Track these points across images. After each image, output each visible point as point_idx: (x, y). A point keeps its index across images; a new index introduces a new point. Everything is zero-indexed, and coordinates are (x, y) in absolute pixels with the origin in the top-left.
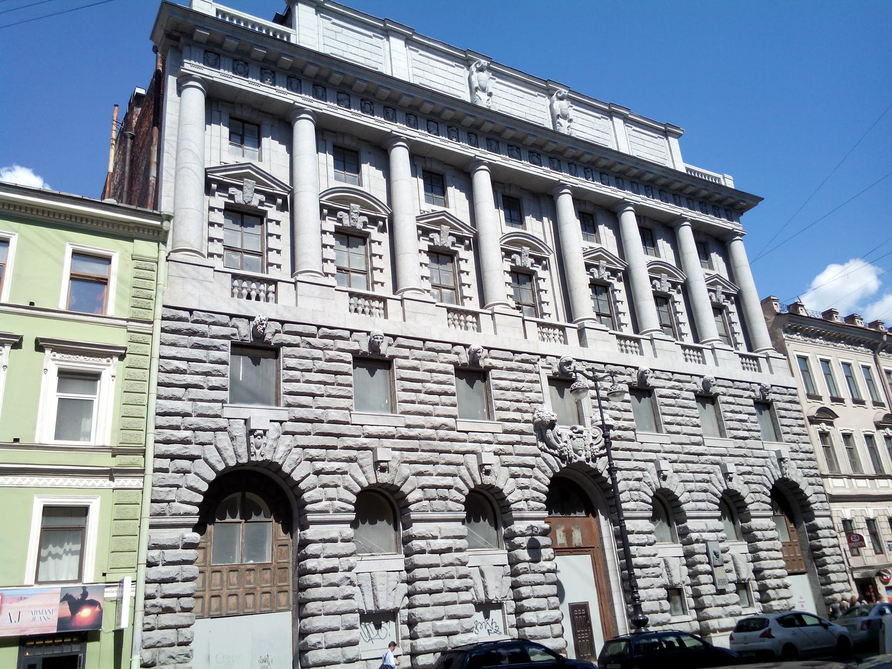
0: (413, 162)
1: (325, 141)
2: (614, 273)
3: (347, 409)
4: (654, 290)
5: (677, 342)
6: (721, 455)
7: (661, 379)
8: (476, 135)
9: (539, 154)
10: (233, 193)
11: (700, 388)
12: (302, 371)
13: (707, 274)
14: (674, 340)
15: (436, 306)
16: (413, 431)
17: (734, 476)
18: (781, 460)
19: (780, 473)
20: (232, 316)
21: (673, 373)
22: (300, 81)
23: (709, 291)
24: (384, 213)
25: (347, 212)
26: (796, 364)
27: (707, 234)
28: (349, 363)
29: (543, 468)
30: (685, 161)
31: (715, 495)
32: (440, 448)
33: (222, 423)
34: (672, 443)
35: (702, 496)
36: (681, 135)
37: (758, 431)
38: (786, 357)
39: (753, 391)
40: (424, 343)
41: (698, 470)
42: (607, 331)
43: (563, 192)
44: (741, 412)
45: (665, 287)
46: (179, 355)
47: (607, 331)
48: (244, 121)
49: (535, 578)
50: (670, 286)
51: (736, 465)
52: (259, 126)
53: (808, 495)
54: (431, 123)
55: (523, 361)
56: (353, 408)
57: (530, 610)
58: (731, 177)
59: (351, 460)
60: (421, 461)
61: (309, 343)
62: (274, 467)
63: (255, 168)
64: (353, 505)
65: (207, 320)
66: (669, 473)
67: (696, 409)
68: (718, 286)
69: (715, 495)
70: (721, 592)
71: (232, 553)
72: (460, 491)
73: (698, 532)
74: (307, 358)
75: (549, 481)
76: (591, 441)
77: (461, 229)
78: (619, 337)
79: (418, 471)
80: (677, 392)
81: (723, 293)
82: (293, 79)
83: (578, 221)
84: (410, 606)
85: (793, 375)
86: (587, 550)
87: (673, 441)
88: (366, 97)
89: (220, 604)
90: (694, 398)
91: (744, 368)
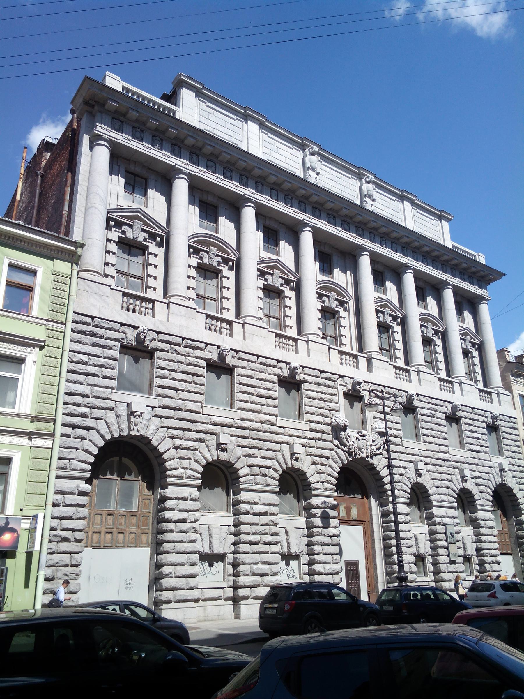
3: (200, 402)
6: (461, 462)
7: (423, 401)
9: (349, 223)
10: (125, 230)
17: (469, 478)
18: (502, 470)
19: (500, 480)
20: (122, 324)
21: (431, 398)
25: (207, 252)
28: (203, 368)
29: (335, 460)
30: (452, 239)
31: (454, 491)
32: (264, 438)
33: (111, 404)
34: (427, 450)
35: (445, 491)
36: (451, 220)
37: (487, 447)
38: (511, 395)
40: (258, 358)
46: (83, 351)
48: (135, 175)
50: (433, 332)
51: (470, 470)
52: (146, 180)
54: (273, 191)
55: (327, 379)
56: (204, 402)
58: (483, 256)
59: (200, 441)
61: (176, 350)
63: (143, 212)
64: (200, 474)
65: (104, 325)
66: (423, 472)
67: (445, 426)
68: (468, 337)
69: (454, 491)
72: (276, 470)
74: (174, 361)
77: (154, 226)
80: (433, 412)
85: (515, 408)
89: (100, 538)
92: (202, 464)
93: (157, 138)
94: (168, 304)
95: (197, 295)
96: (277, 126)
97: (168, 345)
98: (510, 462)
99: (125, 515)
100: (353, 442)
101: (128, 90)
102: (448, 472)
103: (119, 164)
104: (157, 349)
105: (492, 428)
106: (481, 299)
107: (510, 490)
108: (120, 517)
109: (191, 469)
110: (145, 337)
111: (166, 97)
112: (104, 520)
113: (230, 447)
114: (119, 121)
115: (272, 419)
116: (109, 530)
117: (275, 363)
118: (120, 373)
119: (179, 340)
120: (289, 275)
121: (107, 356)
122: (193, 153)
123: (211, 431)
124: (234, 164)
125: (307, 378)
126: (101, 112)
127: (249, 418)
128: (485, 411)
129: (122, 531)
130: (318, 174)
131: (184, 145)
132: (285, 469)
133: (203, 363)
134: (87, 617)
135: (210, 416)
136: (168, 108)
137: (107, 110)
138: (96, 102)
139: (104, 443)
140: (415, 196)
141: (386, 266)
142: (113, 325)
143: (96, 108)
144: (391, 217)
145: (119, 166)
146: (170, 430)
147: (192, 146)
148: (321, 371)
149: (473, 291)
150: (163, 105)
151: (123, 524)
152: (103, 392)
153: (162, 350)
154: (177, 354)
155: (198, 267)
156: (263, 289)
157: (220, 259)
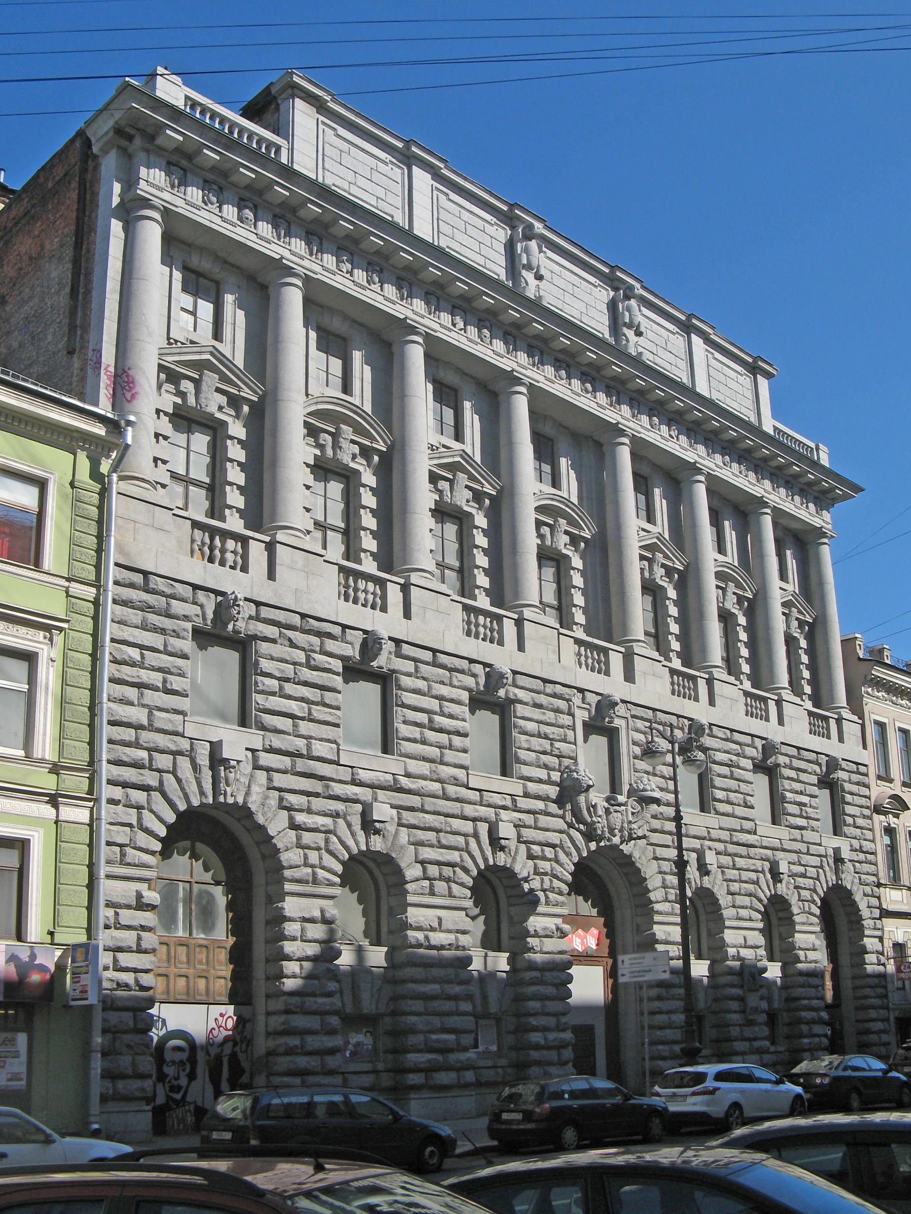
0: (169, 249)
1: (172, 257)
2: (234, 402)
3: (335, 742)
4: (179, 401)
5: (740, 687)
6: (773, 849)
7: (717, 737)
8: (514, 337)
9: (594, 379)
10: (185, 390)
11: (352, 651)
12: (279, 679)
13: (643, 530)
14: (737, 683)
15: (174, 515)
16: (414, 783)
17: (785, 878)
18: (838, 860)
19: (834, 878)
20: (196, 587)
21: (732, 730)
22: (289, 223)
23: (642, 558)
24: (587, 532)
26: (871, 731)
27: (725, 500)
28: (338, 674)
29: (567, 850)
30: (775, 416)
31: (760, 901)
32: (445, 811)
33: (185, 745)
34: (720, 828)
35: (746, 901)
36: (773, 375)
37: (818, 820)
38: (860, 722)
39: (475, 676)
41: (745, 867)
42: (660, 662)
43: (139, 213)
44: (801, 793)
45: (462, 498)
46: (131, 639)
47: (660, 662)
48: (199, 274)
49: (547, 991)
50: (735, 601)
51: (789, 863)
52: (217, 283)
53: (650, 887)
55: (555, 696)
56: (340, 741)
57: (536, 1029)
58: (825, 449)
59: (336, 815)
60: (422, 825)
61: (290, 640)
62: (244, 812)
63: (218, 355)
64: (339, 876)
65: (165, 590)
66: (713, 868)
68: (793, 609)
69: (760, 901)
70: (751, 1023)
71: (176, 928)
72: (466, 870)
73: (735, 947)
74: (287, 662)
75: (573, 868)
76: (630, 818)
77: (239, 383)
78: (466, 608)
79: (418, 838)
80: (734, 758)
81: (663, 566)
82: (281, 220)
83: (532, 446)
84: (394, 1013)
85: (865, 747)
86: (600, 959)
87: (722, 825)
88: (375, 259)
90: (341, 670)
91: (673, 693)
92: (341, 858)
93: (248, 203)
94: (307, 573)
95: (315, 524)
96: (465, 179)
97: (275, 630)
98: (851, 846)
99: (207, 947)
100: (600, 816)
101: (194, 104)
102: (753, 868)
103: (171, 254)
104: (255, 637)
105: (827, 782)
106: (819, 533)
107: (849, 893)
108: (198, 949)
109: (323, 868)
110: (239, 613)
111: (253, 111)
112: (173, 954)
113: (391, 828)
114: (179, 170)
115: (461, 774)
116: (183, 971)
117: (464, 664)
118: (193, 683)
119: (296, 620)
120: (482, 483)
121: (173, 651)
122: (312, 234)
123: (354, 797)
124: (260, 193)
125: (521, 694)
126: (148, 151)
127: (421, 773)
128: (817, 753)
129: (204, 974)
130: (539, 277)
131: (298, 217)
132: (482, 867)
133: (337, 665)
134: (39, 926)
135: (352, 767)
136: (266, 140)
137: (159, 147)
138: (138, 130)
139: (175, 816)
140: (713, 328)
141: (656, 467)
142: (180, 589)
143: (138, 141)
144: (668, 367)
145: (172, 257)
146: (287, 796)
147: (245, 187)
148: (545, 681)
149: (806, 520)
150: (257, 135)
151: (204, 961)
152: (170, 721)
153: (266, 639)
154: (290, 647)
155: (315, 465)
156: (434, 510)
157: (356, 449)
